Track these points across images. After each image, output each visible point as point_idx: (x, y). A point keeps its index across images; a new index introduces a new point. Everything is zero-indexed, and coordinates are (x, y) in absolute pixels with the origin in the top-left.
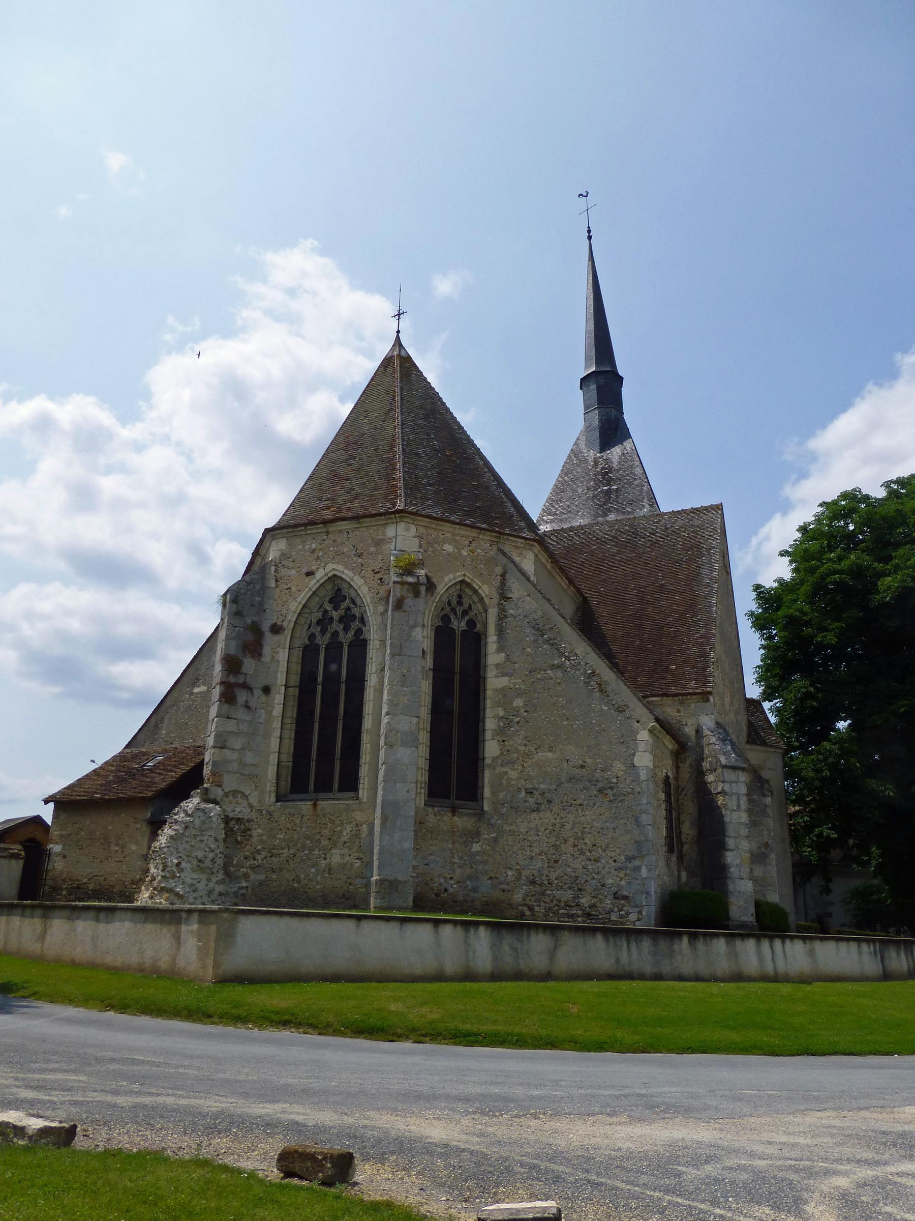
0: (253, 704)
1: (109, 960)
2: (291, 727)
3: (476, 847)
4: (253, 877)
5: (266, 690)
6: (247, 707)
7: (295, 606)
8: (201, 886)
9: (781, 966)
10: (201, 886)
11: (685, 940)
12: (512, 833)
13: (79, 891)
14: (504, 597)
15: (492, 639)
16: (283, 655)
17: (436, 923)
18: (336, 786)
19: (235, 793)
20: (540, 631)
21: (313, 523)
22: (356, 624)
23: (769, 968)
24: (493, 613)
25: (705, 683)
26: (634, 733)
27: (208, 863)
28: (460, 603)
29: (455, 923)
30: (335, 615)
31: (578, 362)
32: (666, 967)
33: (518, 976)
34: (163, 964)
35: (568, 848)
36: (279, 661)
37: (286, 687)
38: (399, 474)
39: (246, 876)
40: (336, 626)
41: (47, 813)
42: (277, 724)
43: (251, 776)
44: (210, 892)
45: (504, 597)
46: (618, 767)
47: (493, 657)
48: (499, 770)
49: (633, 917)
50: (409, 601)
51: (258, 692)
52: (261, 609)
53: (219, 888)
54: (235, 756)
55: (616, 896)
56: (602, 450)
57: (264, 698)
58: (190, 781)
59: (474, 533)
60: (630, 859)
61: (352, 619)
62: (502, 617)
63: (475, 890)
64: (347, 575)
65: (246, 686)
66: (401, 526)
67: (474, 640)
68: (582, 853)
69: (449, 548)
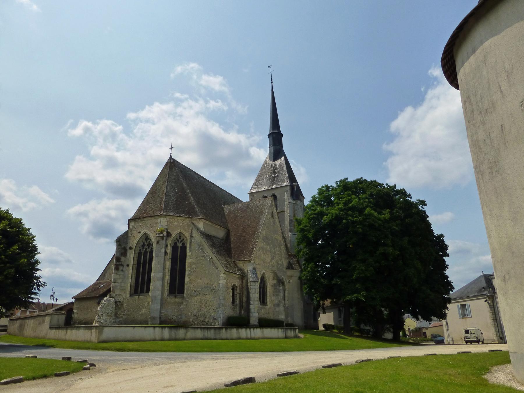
0: (124, 270)
1: (79, 339)
2: (134, 275)
3: (182, 307)
4: (124, 317)
5: (128, 266)
6: (122, 271)
7: (135, 242)
8: (108, 320)
9: (253, 336)
10: (108, 320)
11: (224, 329)
12: (191, 302)
13: (81, 323)
14: (191, 236)
15: (188, 248)
16: (132, 256)
17: (154, 327)
18: (145, 291)
19: (119, 295)
20: (199, 246)
21: (140, 218)
22: (151, 246)
23: (249, 336)
24: (189, 241)
25: (250, 257)
26: (220, 275)
27: (110, 314)
28: (180, 238)
29: (159, 327)
30: (146, 244)
31: (267, 129)
32: (218, 336)
33: (176, 339)
34: (89, 340)
35: (203, 306)
36: (131, 257)
37: (133, 264)
38: (163, 203)
39: (122, 317)
40: (146, 247)
41: (73, 300)
42: (130, 275)
43: (123, 290)
44: (110, 322)
45: (191, 236)
46: (216, 284)
47: (188, 254)
48: (188, 285)
49: (217, 324)
50: (161, 241)
51: (125, 266)
52: (127, 243)
53: (113, 321)
54: (119, 284)
55: (214, 319)
56: (274, 161)
57: (127, 268)
58: (107, 292)
59: (184, 218)
60: (217, 308)
61: (150, 245)
62: (191, 242)
63: (181, 318)
64: (148, 233)
65: (122, 265)
66: (162, 218)
67: (184, 248)
68: (206, 307)
69: (176, 223)
